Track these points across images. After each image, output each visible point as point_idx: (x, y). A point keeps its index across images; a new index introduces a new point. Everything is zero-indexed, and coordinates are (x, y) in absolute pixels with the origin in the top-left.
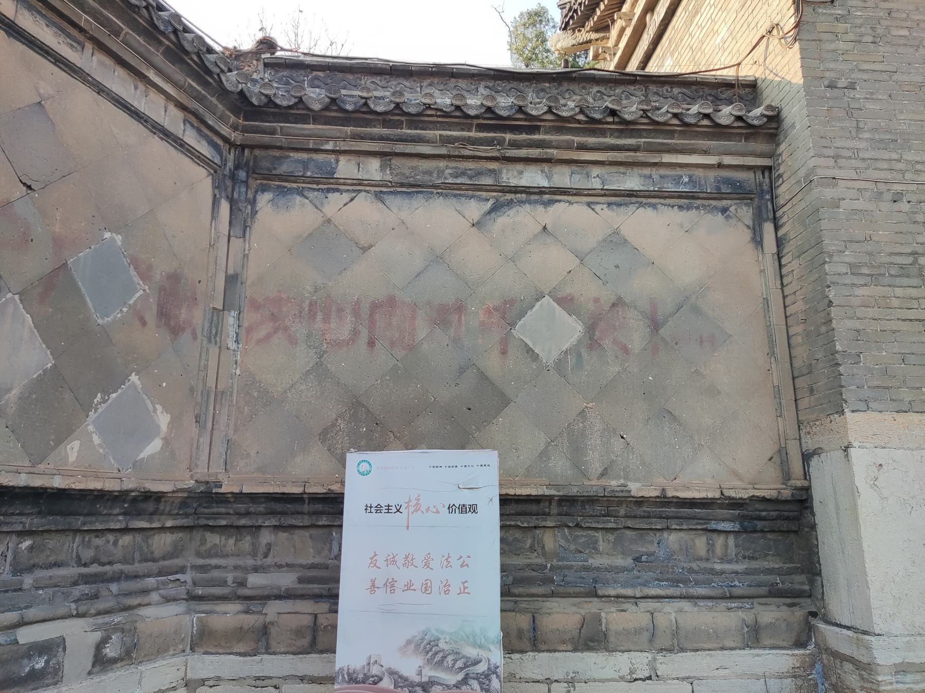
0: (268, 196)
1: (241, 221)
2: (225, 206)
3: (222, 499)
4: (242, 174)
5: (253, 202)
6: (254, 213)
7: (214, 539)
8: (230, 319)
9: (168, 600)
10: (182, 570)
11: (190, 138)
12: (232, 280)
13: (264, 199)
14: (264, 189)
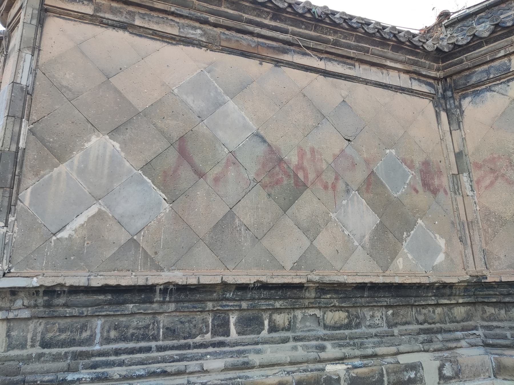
0: (468, 99)
1: (456, 119)
2: (444, 115)
3: (490, 286)
4: (449, 93)
5: (460, 106)
6: (462, 112)
7: (490, 310)
8: (464, 178)
9: (472, 345)
10: (475, 328)
11: (416, 86)
12: (459, 156)
13: (466, 103)
14: (464, 97)
